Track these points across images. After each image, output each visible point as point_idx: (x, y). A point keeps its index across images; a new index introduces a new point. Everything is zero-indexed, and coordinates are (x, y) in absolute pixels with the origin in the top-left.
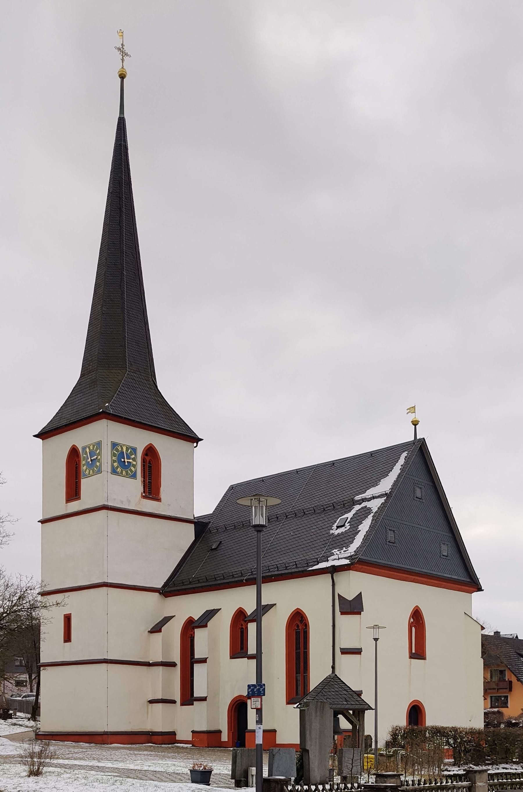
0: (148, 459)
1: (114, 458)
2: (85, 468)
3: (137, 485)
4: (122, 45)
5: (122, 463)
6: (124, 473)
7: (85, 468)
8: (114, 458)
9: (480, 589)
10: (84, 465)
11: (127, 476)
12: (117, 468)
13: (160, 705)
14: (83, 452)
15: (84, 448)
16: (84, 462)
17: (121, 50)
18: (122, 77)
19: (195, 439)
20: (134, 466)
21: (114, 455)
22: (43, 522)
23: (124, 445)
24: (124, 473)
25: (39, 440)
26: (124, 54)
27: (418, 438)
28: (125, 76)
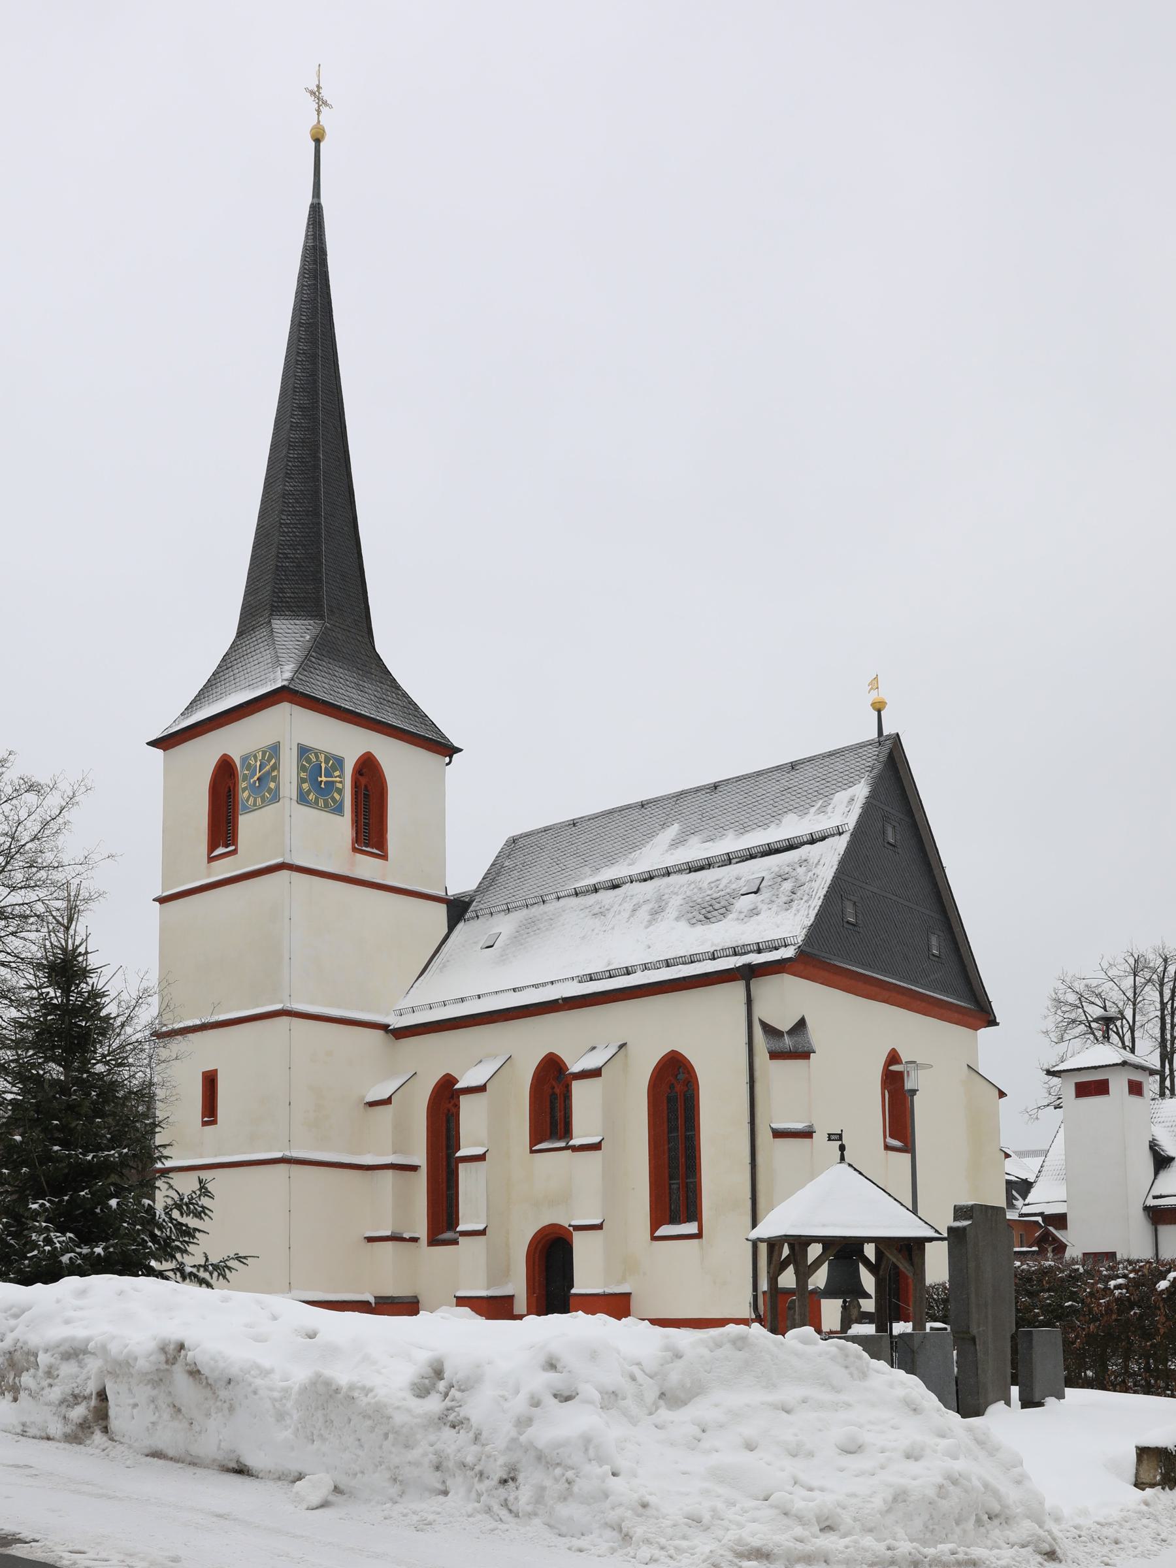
0: (363, 781)
1: (303, 775)
2: (246, 794)
3: (342, 826)
4: (318, 87)
5: (316, 780)
6: (321, 803)
7: (246, 794)
8: (303, 775)
9: (993, 1022)
10: (244, 790)
11: (326, 808)
12: (309, 792)
13: (390, 1244)
14: (242, 766)
15: (244, 759)
16: (244, 785)
17: (316, 93)
18: (318, 141)
19: (447, 750)
20: (340, 791)
21: (302, 768)
22: (162, 900)
23: (321, 752)
24: (321, 803)
25: (158, 753)
26: (321, 102)
27: (885, 733)
28: (323, 137)
